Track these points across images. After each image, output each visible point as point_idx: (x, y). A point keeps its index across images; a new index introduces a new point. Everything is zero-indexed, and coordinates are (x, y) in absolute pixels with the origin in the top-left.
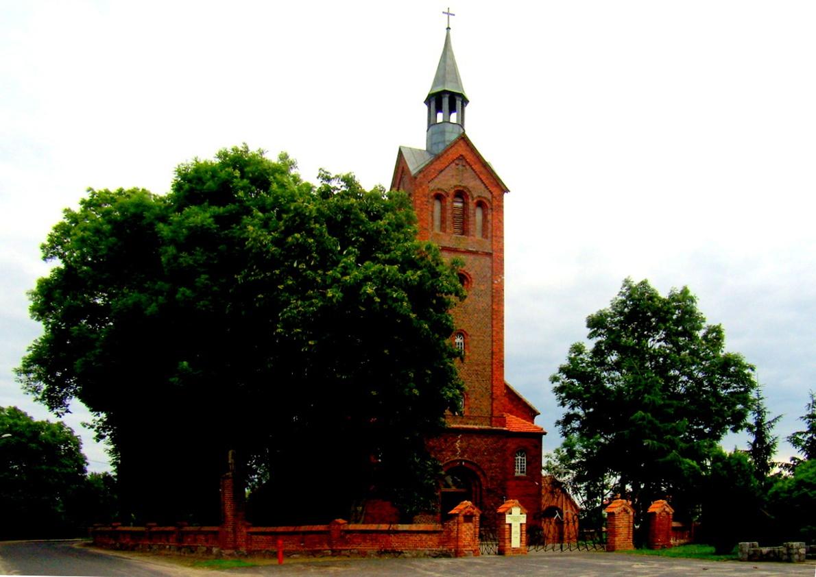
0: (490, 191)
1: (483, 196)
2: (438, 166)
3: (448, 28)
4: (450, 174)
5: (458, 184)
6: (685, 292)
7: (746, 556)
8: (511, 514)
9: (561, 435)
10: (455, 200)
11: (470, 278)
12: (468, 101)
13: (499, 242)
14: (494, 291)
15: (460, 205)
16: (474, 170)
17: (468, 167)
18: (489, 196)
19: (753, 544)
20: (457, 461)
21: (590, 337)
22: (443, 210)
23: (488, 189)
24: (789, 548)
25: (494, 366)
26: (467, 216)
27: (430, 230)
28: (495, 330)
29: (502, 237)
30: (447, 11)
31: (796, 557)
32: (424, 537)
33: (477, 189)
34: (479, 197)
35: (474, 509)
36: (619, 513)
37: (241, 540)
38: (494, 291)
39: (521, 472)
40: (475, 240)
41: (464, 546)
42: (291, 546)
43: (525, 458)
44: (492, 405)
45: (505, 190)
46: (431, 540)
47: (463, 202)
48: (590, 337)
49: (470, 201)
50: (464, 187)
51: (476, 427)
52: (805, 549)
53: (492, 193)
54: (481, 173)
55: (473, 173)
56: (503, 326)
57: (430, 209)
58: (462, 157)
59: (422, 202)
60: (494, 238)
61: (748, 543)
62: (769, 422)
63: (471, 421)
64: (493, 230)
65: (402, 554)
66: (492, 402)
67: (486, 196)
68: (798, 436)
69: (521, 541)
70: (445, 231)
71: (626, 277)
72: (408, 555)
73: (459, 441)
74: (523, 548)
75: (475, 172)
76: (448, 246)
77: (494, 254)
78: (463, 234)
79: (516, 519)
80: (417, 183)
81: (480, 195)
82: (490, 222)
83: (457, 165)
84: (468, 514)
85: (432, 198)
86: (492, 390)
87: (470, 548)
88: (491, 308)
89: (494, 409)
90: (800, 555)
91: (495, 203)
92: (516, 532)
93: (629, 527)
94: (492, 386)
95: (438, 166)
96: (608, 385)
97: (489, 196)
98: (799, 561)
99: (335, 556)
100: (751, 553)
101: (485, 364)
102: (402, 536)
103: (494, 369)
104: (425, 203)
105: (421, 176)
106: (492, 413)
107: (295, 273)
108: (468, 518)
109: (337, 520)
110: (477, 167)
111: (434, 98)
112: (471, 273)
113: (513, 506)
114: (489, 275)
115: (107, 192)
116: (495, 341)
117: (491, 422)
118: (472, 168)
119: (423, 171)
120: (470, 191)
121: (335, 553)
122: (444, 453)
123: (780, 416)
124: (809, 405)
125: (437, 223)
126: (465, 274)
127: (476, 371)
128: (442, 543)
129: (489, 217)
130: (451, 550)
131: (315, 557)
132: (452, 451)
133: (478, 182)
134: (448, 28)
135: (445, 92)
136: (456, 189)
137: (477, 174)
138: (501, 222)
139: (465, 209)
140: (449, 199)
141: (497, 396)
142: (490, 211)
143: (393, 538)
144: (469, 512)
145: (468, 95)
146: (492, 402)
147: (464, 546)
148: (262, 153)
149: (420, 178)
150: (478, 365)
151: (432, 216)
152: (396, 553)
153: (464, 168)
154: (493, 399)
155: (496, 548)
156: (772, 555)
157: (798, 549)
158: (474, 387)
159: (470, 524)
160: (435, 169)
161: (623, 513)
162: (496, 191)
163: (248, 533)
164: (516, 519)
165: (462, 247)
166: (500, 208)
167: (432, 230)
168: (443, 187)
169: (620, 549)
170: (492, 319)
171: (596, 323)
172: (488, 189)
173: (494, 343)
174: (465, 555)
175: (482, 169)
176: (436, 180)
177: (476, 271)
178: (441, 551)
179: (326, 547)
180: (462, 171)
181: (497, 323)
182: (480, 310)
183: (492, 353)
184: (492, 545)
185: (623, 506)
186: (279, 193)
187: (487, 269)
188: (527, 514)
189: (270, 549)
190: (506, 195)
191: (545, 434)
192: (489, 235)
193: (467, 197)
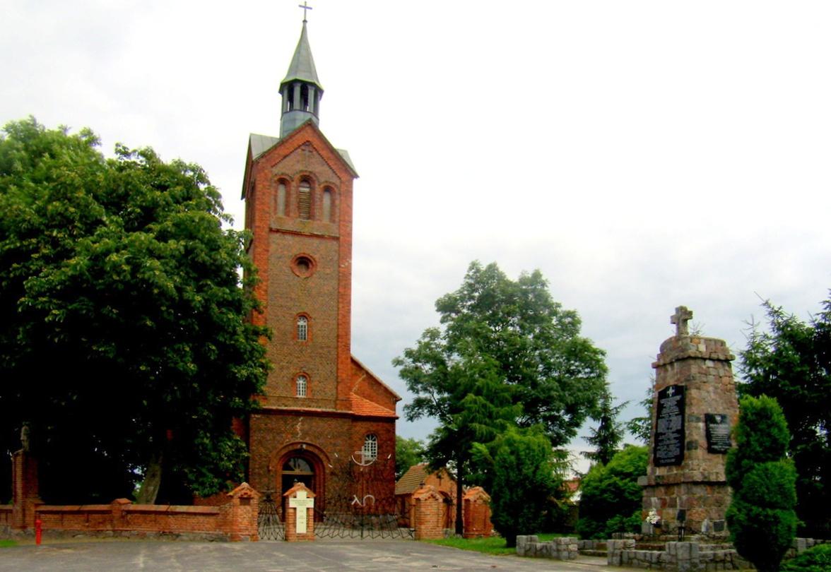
1: (331, 181)
2: (283, 151)
3: (305, 21)
6: (537, 276)
7: (522, 551)
8: (295, 497)
9: (407, 419)
10: (302, 184)
13: (348, 226)
14: (341, 274)
15: (307, 190)
16: (321, 156)
17: (315, 153)
18: (338, 182)
19: (531, 538)
20: (299, 443)
21: (442, 322)
22: (288, 195)
23: (336, 174)
24: (558, 544)
25: (340, 349)
26: (314, 201)
27: (272, 214)
29: (351, 222)
30: (304, 5)
31: (565, 554)
32: (201, 519)
33: (323, 173)
34: (326, 182)
35: (251, 491)
36: (426, 500)
37: (30, 519)
38: (341, 274)
39: (372, 456)
40: (321, 223)
41: (240, 530)
42: (76, 526)
43: (376, 442)
44: (337, 388)
46: (208, 523)
47: (310, 187)
48: (442, 322)
49: (317, 186)
50: (311, 172)
51: (319, 410)
52: (576, 546)
53: (340, 179)
54: (328, 158)
55: (321, 159)
57: (273, 192)
58: (307, 143)
59: (264, 186)
60: (341, 223)
61: (524, 537)
62: (616, 408)
63: (314, 404)
64: (342, 216)
65: (180, 537)
66: (337, 385)
67: (334, 181)
68: (637, 422)
69: (308, 527)
70: (288, 216)
71: (474, 260)
72: (185, 538)
73: (300, 423)
74: (309, 534)
76: (291, 229)
77: (341, 238)
78: (309, 218)
80: (259, 168)
81: (328, 180)
83: (303, 150)
84: (245, 496)
85: (275, 182)
86: (337, 373)
87: (247, 533)
88: (336, 292)
89: (339, 392)
90: (570, 552)
91: (343, 188)
92: (302, 517)
93: (438, 515)
94: (338, 369)
95: (283, 151)
96: (214, 348)
97: (338, 182)
98: (569, 558)
99: (117, 537)
100: (528, 547)
101: (330, 347)
102: (180, 516)
103: (340, 352)
104: (268, 187)
105: (264, 160)
106: (337, 397)
107: (55, 242)
108: (245, 500)
110: (325, 153)
111: (286, 87)
112: (317, 257)
113: (298, 490)
114: (336, 258)
115: (505, 276)
116: (341, 324)
117: (336, 404)
118: (319, 154)
120: (316, 176)
121: (117, 534)
122: (284, 435)
123: (628, 402)
124: (650, 389)
125: (281, 207)
126: (309, 257)
127: (320, 354)
128: (219, 526)
129: (337, 202)
130: (226, 534)
131: (97, 538)
132: (292, 434)
134: (305, 21)
135: (296, 81)
136: (301, 174)
138: (350, 207)
139: (311, 195)
140: (294, 184)
141: (343, 380)
142: (337, 196)
143: (171, 519)
144: (246, 494)
145: (323, 83)
146: (337, 385)
147: (240, 530)
148: (65, 130)
149: (263, 163)
150: (322, 348)
151: (276, 201)
152: (175, 536)
153: (310, 154)
154: (338, 382)
155: (282, 533)
156: (544, 551)
157: (567, 545)
158: (318, 370)
159: (248, 508)
160: (278, 154)
161: (431, 500)
162: (345, 177)
163: (36, 511)
165: (307, 231)
167: (275, 214)
168: (287, 172)
169: (427, 538)
170: (338, 302)
171: (446, 306)
172: (336, 174)
173: (340, 327)
174: (241, 540)
175: (330, 155)
177: (321, 255)
178: (217, 535)
179: (109, 527)
180: (309, 156)
181: (343, 307)
182: (325, 294)
183: (338, 336)
184: (279, 528)
185: (431, 492)
186: (50, 164)
187: (334, 253)
188: (315, 499)
189: (56, 528)
190: (355, 181)
191: (397, 418)
192: (337, 220)
193: (314, 182)
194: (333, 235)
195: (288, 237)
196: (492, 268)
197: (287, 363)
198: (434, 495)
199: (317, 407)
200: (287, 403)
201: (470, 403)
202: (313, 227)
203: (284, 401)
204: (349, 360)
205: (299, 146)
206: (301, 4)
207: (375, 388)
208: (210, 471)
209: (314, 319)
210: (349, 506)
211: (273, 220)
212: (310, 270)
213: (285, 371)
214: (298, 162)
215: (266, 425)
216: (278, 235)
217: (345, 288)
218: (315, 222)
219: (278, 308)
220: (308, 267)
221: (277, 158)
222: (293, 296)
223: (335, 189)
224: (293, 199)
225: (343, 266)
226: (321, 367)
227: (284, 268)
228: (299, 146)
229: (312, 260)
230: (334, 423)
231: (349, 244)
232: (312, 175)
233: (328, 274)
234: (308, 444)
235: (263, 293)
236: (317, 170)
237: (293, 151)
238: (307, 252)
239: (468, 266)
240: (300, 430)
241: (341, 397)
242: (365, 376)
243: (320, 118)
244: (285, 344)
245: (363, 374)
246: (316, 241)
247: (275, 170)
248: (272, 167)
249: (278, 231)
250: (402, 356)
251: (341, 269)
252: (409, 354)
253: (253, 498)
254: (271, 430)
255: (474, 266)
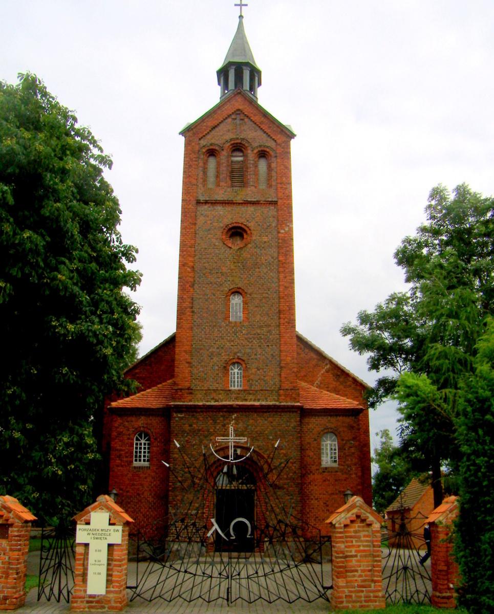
0: (273, 139)
3: (241, 17)
4: (225, 129)
5: (235, 137)
8: (88, 523)
10: (234, 154)
11: (250, 230)
13: (286, 189)
15: (241, 159)
17: (246, 120)
22: (218, 165)
23: (271, 137)
28: (283, 285)
33: (255, 137)
43: (336, 443)
45: (290, 135)
51: (257, 403)
55: (254, 125)
56: (293, 279)
58: (239, 112)
63: (251, 397)
67: (269, 145)
69: (109, 582)
71: (435, 185)
75: (255, 123)
77: (280, 202)
79: (99, 535)
82: (275, 170)
110: (257, 118)
112: (251, 225)
117: (279, 395)
119: (192, 129)
126: (243, 226)
129: (273, 165)
133: (260, 133)
134: (241, 17)
137: (257, 125)
138: (288, 168)
141: (287, 364)
145: (259, 64)
150: (261, 327)
153: (241, 122)
154: (281, 368)
162: (280, 138)
164: (99, 535)
165: (239, 199)
166: (286, 154)
170: (279, 272)
172: (271, 137)
176: (208, 137)
180: (240, 124)
183: (280, 312)
185: (355, 511)
192: (274, 183)
194: (270, 200)
195: (219, 208)
196: (462, 191)
197: (218, 348)
198: (363, 516)
199: (255, 400)
200: (217, 398)
201: (438, 359)
202: (249, 194)
203: (214, 395)
204: (295, 339)
205: (229, 116)
206: (237, 3)
207: (341, 380)
208: (31, 482)
209: (250, 295)
210: (204, 541)
211: (201, 191)
212: (244, 240)
213: (215, 359)
214: (229, 131)
215: (190, 426)
216: (206, 207)
217: (286, 255)
218: (249, 189)
219: (207, 286)
220: (242, 236)
221: (205, 130)
222: (225, 270)
223: (271, 152)
224: (224, 169)
225: (282, 231)
226: (259, 350)
227: (214, 240)
228: (229, 116)
229: (246, 229)
231: (290, 207)
232: (244, 143)
233: (265, 242)
235: (189, 269)
236: (249, 137)
237: (222, 121)
238: (240, 221)
239: (427, 194)
241: (287, 386)
242: (328, 366)
243: (258, 97)
244: (215, 326)
245: (327, 364)
246: (251, 209)
247: (203, 142)
248: (200, 139)
249: (206, 202)
250: (355, 323)
251: (280, 235)
252: (364, 319)
253: (12, 525)
254: (194, 432)
255: (437, 194)
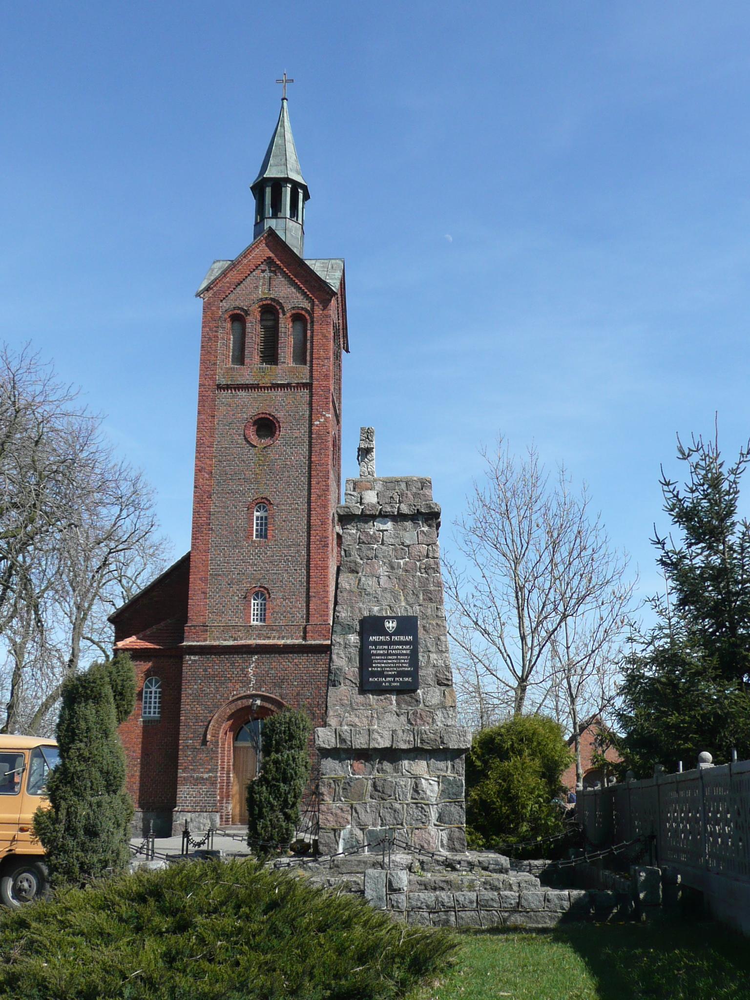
2: (233, 277)
12: (252, 188)
51: (281, 642)
63: (274, 634)
104: (214, 329)
109: (232, 721)
135: (288, 180)
158: (281, 581)
176: (232, 296)
195: (242, 393)
230: (302, 660)
234: (264, 698)
236: (282, 294)
240: (254, 675)
249: (227, 387)
